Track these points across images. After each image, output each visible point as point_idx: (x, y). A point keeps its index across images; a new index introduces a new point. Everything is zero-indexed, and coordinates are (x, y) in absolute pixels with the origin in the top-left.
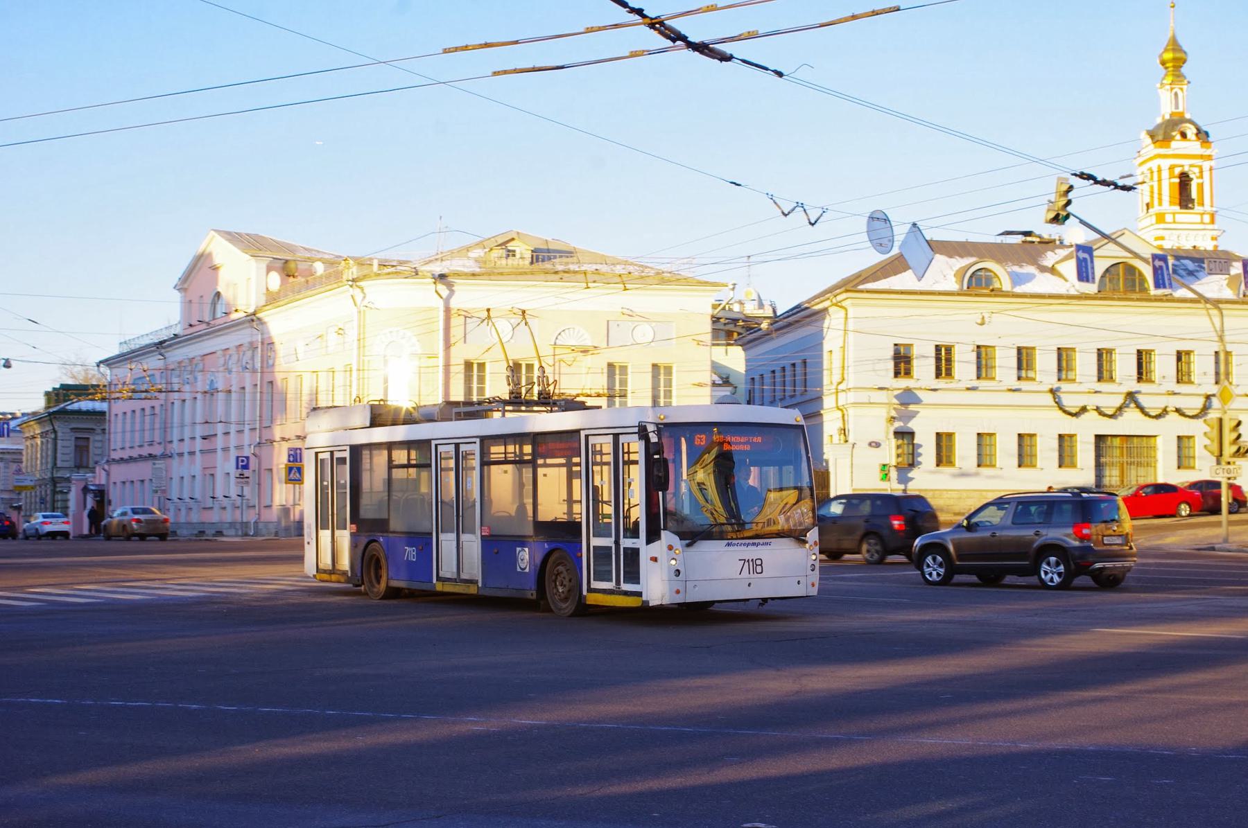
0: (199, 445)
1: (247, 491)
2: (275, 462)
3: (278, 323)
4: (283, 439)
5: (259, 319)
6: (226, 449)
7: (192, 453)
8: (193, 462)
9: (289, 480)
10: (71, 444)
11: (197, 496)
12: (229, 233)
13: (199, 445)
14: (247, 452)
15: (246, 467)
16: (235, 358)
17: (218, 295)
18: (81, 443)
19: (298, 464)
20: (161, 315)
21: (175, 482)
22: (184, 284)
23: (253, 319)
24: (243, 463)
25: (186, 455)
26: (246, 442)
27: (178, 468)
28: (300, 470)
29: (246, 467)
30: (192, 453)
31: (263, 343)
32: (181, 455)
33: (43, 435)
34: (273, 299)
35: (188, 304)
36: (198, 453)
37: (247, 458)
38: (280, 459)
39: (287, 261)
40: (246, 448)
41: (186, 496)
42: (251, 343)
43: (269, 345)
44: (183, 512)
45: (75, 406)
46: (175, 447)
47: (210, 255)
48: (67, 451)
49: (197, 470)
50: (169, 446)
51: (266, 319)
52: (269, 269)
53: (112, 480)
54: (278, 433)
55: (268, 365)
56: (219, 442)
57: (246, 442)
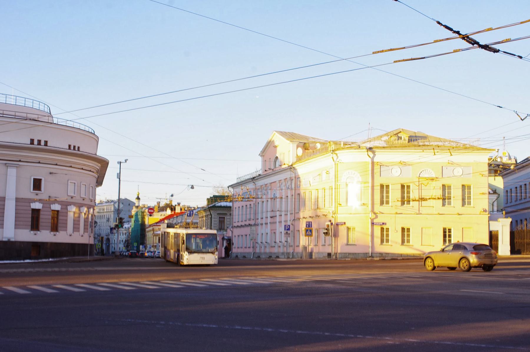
0: (269, 220)
1: (289, 239)
3: (302, 169)
5: (294, 168)
6: (280, 222)
7: (266, 224)
8: (267, 227)
9: (306, 235)
10: (218, 220)
11: (269, 241)
12: (281, 132)
13: (269, 220)
15: (289, 229)
16: (284, 184)
17: (277, 158)
18: (223, 219)
19: (310, 228)
20: (254, 166)
22: (263, 154)
23: (291, 168)
24: (287, 228)
25: (264, 224)
26: (289, 219)
27: (261, 230)
28: (311, 231)
29: (289, 229)
31: (295, 177)
32: (262, 224)
34: (299, 159)
35: (264, 162)
36: (269, 224)
38: (303, 226)
39: (305, 143)
40: (289, 221)
41: (264, 242)
42: (291, 178)
43: (297, 178)
44: (263, 248)
45: (219, 204)
46: (259, 221)
47: (273, 141)
48: (216, 222)
50: (257, 221)
51: (296, 168)
52: (298, 147)
53: (234, 235)
54: (301, 215)
55: (298, 187)
56: (278, 219)
57: (289, 219)
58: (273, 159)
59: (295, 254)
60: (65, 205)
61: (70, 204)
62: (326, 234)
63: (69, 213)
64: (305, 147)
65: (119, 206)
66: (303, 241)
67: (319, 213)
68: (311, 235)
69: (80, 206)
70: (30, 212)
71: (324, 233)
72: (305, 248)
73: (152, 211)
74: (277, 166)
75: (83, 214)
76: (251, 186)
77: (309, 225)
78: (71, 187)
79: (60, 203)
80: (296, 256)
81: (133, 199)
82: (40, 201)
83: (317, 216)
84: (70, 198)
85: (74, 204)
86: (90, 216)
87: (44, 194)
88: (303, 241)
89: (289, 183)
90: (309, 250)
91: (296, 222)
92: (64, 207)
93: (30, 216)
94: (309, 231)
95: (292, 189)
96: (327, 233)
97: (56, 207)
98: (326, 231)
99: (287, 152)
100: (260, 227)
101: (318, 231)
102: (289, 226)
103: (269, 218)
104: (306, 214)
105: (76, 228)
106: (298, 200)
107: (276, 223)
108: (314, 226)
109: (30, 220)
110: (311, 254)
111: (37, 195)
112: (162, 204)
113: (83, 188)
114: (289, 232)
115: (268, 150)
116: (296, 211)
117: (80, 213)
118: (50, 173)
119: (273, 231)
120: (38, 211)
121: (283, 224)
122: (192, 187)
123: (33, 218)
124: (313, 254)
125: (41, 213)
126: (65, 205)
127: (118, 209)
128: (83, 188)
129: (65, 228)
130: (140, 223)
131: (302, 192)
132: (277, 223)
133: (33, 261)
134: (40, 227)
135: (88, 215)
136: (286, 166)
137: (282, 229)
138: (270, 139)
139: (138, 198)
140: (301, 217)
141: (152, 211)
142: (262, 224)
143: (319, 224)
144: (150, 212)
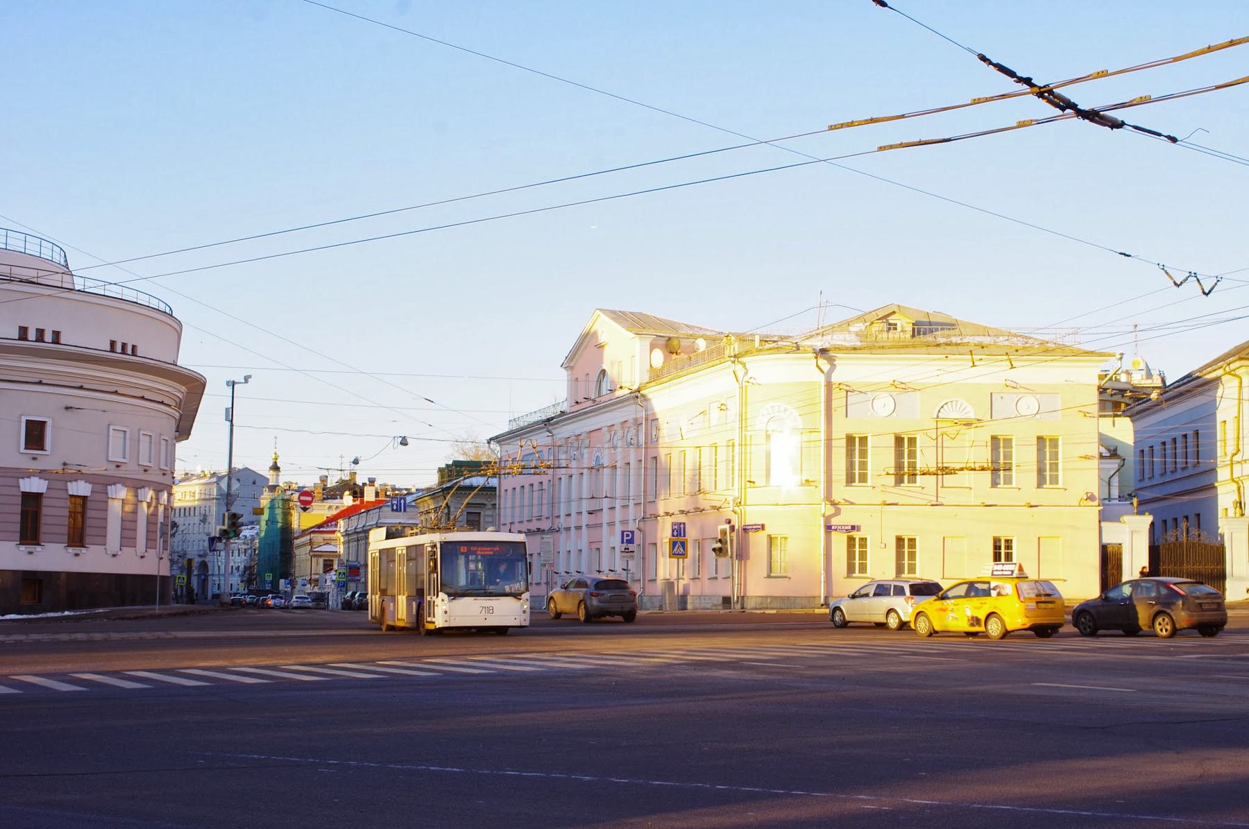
2: (659, 536)
3: (662, 400)
4: (667, 514)
5: (643, 396)
6: (611, 524)
7: (579, 528)
8: (579, 537)
13: (585, 518)
14: (632, 526)
15: (631, 541)
16: (620, 434)
17: (603, 372)
19: (681, 539)
20: (549, 392)
21: (563, 556)
22: (570, 363)
23: (637, 396)
24: (628, 538)
25: (573, 529)
26: (631, 517)
27: (567, 543)
28: (683, 544)
29: (631, 541)
30: (579, 528)
31: (647, 419)
32: (568, 529)
33: (436, 510)
34: (656, 376)
37: (632, 532)
38: (664, 533)
39: (670, 339)
40: (631, 522)
43: (652, 420)
46: (562, 522)
47: (595, 333)
49: (584, 544)
50: (557, 521)
51: (650, 396)
54: (661, 508)
55: (652, 441)
56: (605, 517)
57: (631, 517)
58: (594, 377)
59: (645, 599)
60: (103, 483)
61: (115, 481)
62: (719, 551)
63: (110, 501)
64: (670, 347)
65: (229, 486)
66: (666, 568)
67: (703, 502)
68: (684, 555)
69: (136, 486)
70: (68, 503)
71: (714, 550)
72: (670, 585)
73: (309, 499)
74: (604, 391)
75: (145, 505)
76: (542, 439)
77: (679, 530)
78: (115, 440)
79: (89, 478)
80: (649, 605)
81: (263, 469)
82: (42, 474)
83: (699, 510)
84: (113, 467)
85: (124, 481)
86: (161, 509)
87: (51, 458)
88: (666, 568)
89: (633, 431)
90: (679, 588)
91: (649, 523)
92: (99, 488)
93: (18, 509)
94: (678, 546)
95: (638, 446)
96: (720, 549)
97: (81, 488)
98: (719, 545)
99: (627, 359)
100: (562, 536)
101: (700, 544)
102: (632, 532)
103: (585, 514)
104: (671, 503)
105: (128, 538)
106: (654, 472)
107: (600, 525)
108: (692, 534)
109: (18, 518)
110: (683, 599)
111: (34, 459)
112: (331, 483)
113: (144, 442)
114: (631, 547)
115: (585, 350)
116: (650, 498)
117: (138, 502)
118: (67, 408)
119: (594, 546)
120: (38, 496)
121: (618, 528)
122: (404, 442)
123: (24, 514)
124: (689, 600)
125: (45, 502)
126: (103, 483)
127: (229, 494)
128: (144, 442)
129: (102, 538)
130: (279, 525)
131: (662, 453)
132: (605, 526)
133: (25, 616)
134: (42, 537)
135: (156, 507)
136: (625, 392)
137: (616, 540)
138: (586, 330)
139: (276, 468)
140: (661, 512)
141: (309, 499)
142: (568, 529)
143: (702, 529)
144: (302, 502)
